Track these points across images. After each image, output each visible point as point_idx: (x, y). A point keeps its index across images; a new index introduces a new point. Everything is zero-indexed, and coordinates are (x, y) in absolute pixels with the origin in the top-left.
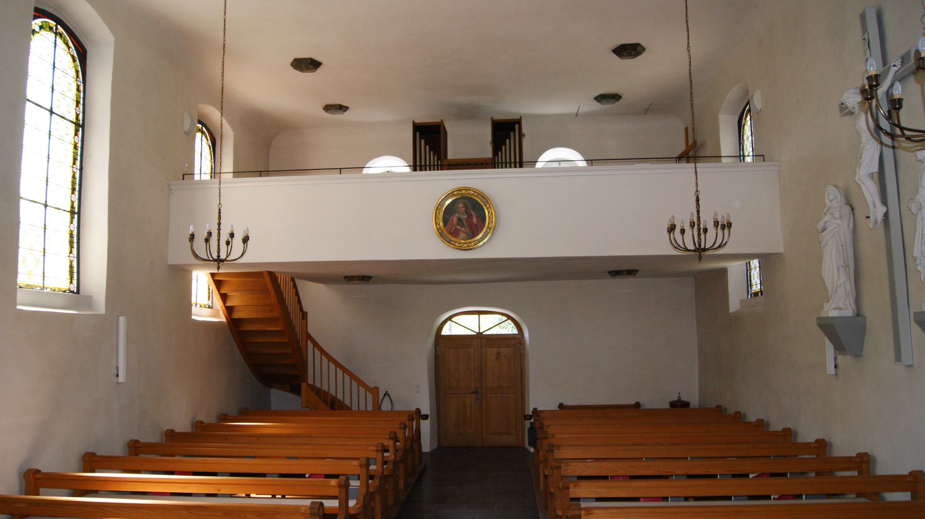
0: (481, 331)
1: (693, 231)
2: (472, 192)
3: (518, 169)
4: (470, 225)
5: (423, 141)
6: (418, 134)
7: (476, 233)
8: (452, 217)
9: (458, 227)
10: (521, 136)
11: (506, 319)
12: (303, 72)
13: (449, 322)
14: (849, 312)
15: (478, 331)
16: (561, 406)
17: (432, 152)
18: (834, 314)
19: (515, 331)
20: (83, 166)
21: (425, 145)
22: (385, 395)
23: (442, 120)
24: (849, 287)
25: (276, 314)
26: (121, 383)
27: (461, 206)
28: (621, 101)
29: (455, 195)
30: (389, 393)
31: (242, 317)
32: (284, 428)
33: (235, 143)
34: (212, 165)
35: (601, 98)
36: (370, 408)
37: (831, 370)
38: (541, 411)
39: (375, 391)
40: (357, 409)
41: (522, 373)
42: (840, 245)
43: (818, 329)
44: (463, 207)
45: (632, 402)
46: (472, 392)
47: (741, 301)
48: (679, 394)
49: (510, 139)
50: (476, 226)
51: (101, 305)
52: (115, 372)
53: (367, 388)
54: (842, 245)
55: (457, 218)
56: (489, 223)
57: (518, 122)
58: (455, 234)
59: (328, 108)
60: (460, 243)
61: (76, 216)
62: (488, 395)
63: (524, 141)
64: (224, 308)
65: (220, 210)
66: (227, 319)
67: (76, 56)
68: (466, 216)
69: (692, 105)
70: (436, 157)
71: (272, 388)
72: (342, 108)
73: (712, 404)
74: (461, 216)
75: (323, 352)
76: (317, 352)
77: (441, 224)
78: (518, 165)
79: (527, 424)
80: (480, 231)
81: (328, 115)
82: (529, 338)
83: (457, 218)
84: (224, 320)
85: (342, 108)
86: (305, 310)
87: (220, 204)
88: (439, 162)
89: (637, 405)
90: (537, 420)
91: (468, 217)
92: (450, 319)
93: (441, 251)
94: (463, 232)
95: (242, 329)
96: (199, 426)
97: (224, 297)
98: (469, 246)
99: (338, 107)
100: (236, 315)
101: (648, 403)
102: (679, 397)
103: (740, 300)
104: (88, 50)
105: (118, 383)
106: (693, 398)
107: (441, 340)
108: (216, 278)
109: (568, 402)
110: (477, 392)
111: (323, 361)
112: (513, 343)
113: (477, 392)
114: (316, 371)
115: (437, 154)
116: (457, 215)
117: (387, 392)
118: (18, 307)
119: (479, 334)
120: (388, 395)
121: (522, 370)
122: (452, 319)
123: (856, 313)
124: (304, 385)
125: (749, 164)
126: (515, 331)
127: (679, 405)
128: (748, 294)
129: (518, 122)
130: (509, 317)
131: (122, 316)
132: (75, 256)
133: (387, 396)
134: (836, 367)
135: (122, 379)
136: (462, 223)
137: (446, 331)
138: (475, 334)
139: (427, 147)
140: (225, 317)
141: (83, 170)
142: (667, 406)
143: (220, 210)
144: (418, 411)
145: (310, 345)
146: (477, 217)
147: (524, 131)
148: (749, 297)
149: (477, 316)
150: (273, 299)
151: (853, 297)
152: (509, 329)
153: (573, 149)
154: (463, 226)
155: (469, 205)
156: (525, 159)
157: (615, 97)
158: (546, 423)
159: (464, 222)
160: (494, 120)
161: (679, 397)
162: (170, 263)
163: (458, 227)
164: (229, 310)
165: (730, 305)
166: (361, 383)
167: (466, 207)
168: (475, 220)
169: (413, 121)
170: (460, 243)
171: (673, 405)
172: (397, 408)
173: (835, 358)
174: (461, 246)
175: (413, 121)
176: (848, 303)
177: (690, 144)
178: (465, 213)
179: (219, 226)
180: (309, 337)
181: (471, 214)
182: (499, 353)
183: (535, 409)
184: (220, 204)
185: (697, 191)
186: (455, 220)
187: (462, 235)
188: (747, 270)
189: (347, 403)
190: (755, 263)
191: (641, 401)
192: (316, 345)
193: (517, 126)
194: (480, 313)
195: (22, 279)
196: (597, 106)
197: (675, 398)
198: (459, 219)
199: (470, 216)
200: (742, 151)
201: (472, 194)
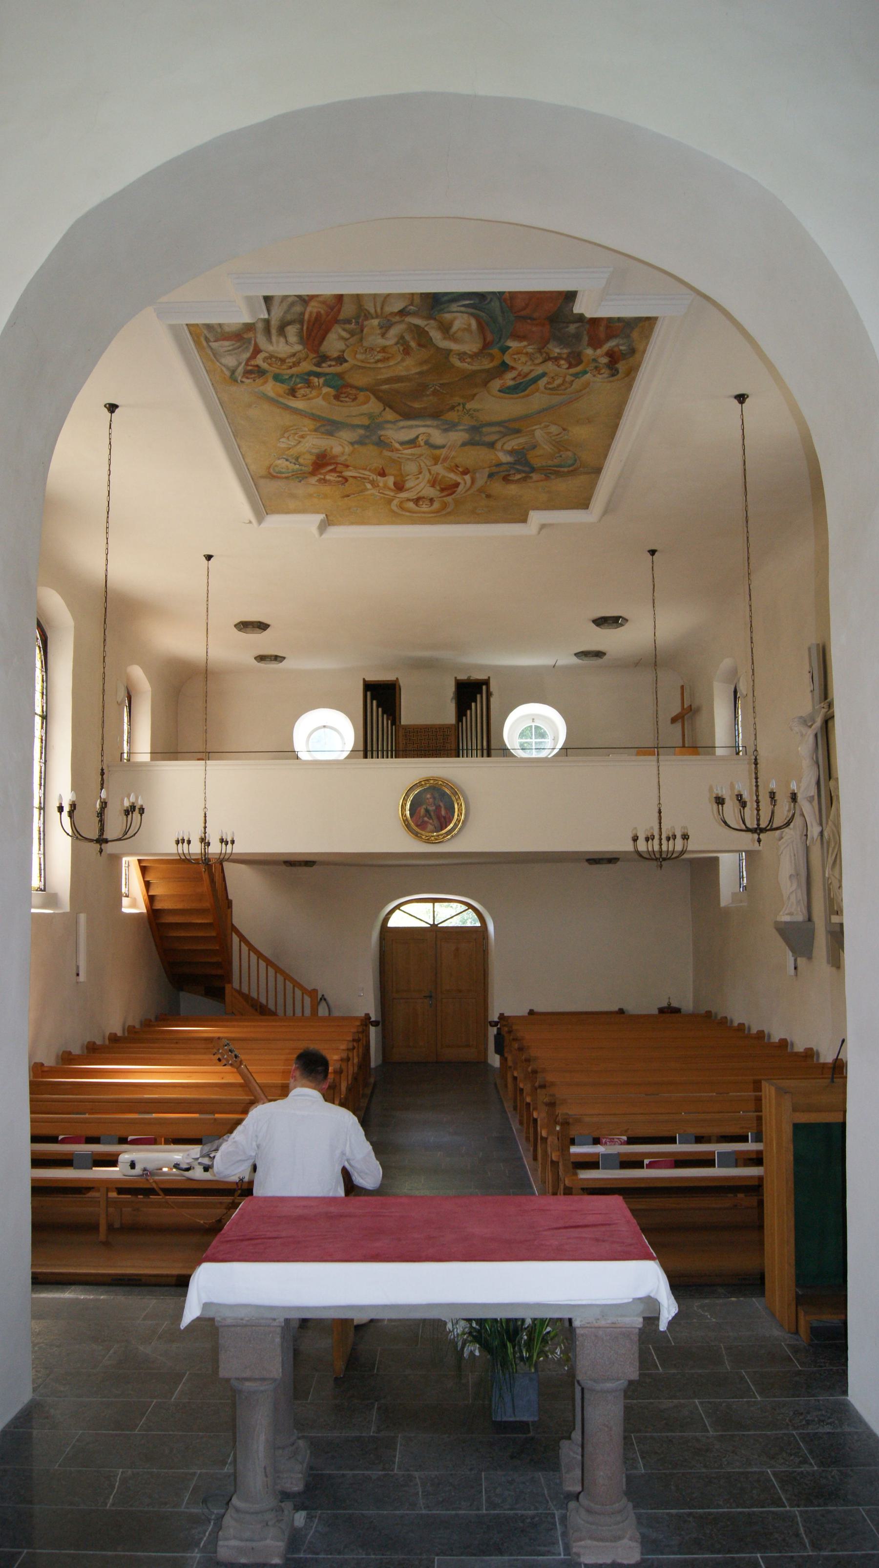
0: (436, 923)
1: (648, 845)
2: (440, 783)
3: (485, 759)
4: (439, 817)
5: (375, 702)
6: (369, 694)
7: (444, 826)
8: (419, 809)
9: (426, 819)
10: (489, 694)
11: (467, 908)
12: (247, 633)
13: (397, 911)
14: (800, 917)
15: (432, 923)
16: (531, 1012)
17: (385, 716)
18: (787, 918)
19: (478, 924)
20: (47, 759)
21: (378, 707)
22: (321, 999)
23: (397, 679)
24: (802, 895)
25: (206, 904)
26: (81, 982)
27: (428, 796)
28: (605, 657)
29: (422, 785)
30: (326, 997)
31: (166, 908)
32: (227, 1032)
33: (152, 701)
34: (43, 676)
35: (583, 654)
36: (308, 1012)
37: (792, 971)
38: (509, 1017)
39: (313, 993)
40: (292, 1014)
41: (484, 975)
42: (792, 855)
43: (774, 931)
44: (430, 798)
45: (615, 1008)
46: (425, 997)
47: (734, 894)
48: (669, 998)
49: (476, 702)
50: (445, 818)
51: (66, 907)
52: (74, 972)
53: (304, 990)
54: (795, 855)
55: (424, 809)
56: (458, 815)
57: (486, 682)
58: (422, 825)
59: (261, 658)
60: (427, 836)
61: (42, 811)
62: (444, 1000)
63: (492, 700)
64: (146, 897)
65: (205, 814)
66: (147, 911)
67: (41, 646)
68: (434, 808)
69: (657, 722)
70: (389, 722)
71: (182, 990)
72: (277, 658)
73: (703, 1010)
74: (428, 807)
75: (251, 948)
76: (245, 948)
77: (408, 813)
78: (485, 752)
79: (493, 1031)
80: (448, 824)
81: (262, 665)
82: (495, 932)
83: (424, 809)
84: (144, 911)
85: (277, 658)
86: (230, 897)
87: (205, 808)
88: (394, 727)
89: (621, 1011)
90: (505, 1025)
91: (436, 808)
92: (398, 907)
93: (405, 843)
94: (431, 824)
95: (164, 921)
96: (131, 1030)
97: (147, 885)
98: (436, 839)
99: (273, 658)
100: (158, 906)
101: (632, 1008)
102: (669, 1002)
103: (732, 893)
104: (48, 637)
105: (77, 983)
106: (686, 1003)
107: (389, 936)
108: (143, 864)
109: (539, 1008)
110: (431, 997)
111: (251, 958)
112: (477, 935)
113: (431, 997)
114: (243, 972)
115: (391, 717)
116: (424, 806)
117: (323, 995)
118: (33, 910)
119: (434, 926)
120: (325, 1000)
121: (484, 971)
122: (401, 908)
123: (807, 917)
124: (228, 987)
125: (723, 758)
126: (478, 924)
127: (669, 1011)
128: (740, 887)
129: (486, 682)
130: (470, 906)
131: (81, 912)
132: (42, 853)
133: (323, 1001)
134: (796, 968)
135: (82, 978)
136: (430, 815)
137: (392, 923)
138: (429, 926)
139: (380, 709)
140: (146, 908)
141: (47, 763)
142: (656, 1012)
143: (205, 814)
144: (367, 1016)
145: (236, 939)
146: (446, 808)
147: (492, 689)
148: (741, 889)
149: (431, 904)
150: (205, 887)
151: (804, 903)
152: (470, 920)
153: (548, 705)
154: (431, 818)
155: (437, 795)
156: (493, 746)
157: (599, 654)
158: (515, 1027)
159: (432, 814)
160: (458, 680)
161: (669, 1002)
162: (108, 852)
163: (426, 819)
164: (151, 899)
165: (721, 900)
166: (296, 984)
167: (434, 798)
168: (443, 813)
169: (364, 679)
170: (427, 836)
171: (662, 1011)
172: (336, 1013)
173: (795, 960)
174: (428, 839)
175: (364, 679)
176: (799, 909)
177: (685, 706)
178: (433, 805)
179: (205, 830)
180: (235, 929)
181: (440, 806)
182: (457, 949)
183: (502, 1016)
184: (205, 808)
185: (660, 804)
186: (423, 811)
187: (430, 827)
188: (740, 860)
189: (271, 1006)
190: (744, 853)
191: (625, 1007)
192: (242, 938)
193: (484, 687)
194: (434, 901)
195: (33, 885)
196: (575, 661)
197: (664, 1004)
198: (427, 811)
199: (438, 808)
200: (737, 726)
201: (441, 784)
